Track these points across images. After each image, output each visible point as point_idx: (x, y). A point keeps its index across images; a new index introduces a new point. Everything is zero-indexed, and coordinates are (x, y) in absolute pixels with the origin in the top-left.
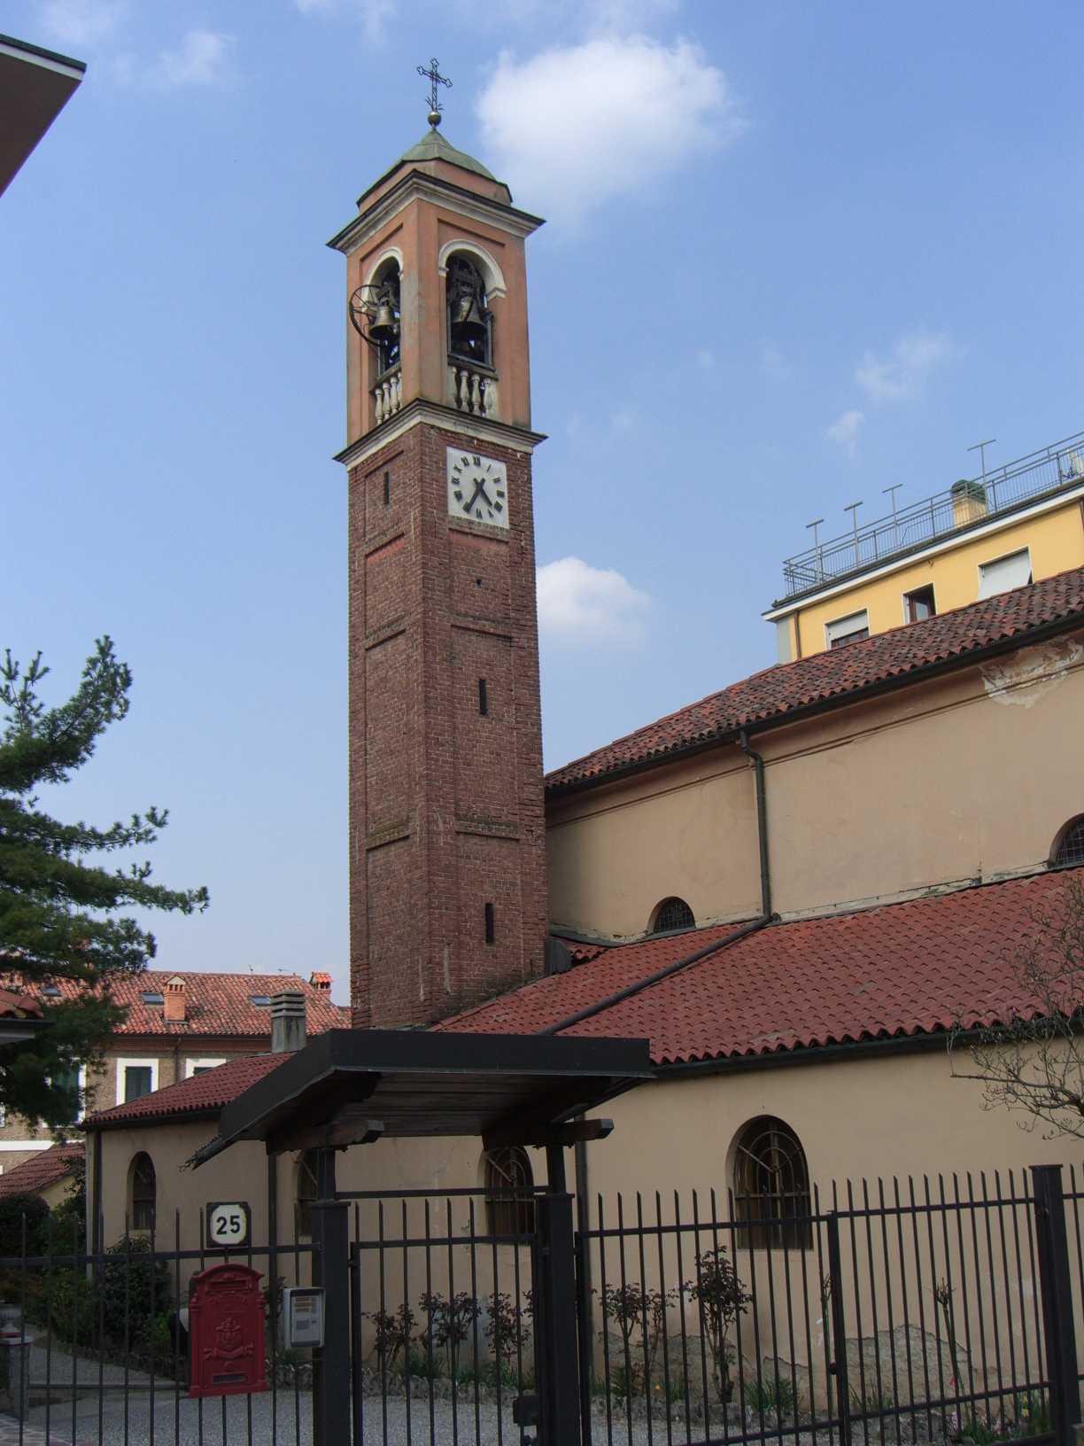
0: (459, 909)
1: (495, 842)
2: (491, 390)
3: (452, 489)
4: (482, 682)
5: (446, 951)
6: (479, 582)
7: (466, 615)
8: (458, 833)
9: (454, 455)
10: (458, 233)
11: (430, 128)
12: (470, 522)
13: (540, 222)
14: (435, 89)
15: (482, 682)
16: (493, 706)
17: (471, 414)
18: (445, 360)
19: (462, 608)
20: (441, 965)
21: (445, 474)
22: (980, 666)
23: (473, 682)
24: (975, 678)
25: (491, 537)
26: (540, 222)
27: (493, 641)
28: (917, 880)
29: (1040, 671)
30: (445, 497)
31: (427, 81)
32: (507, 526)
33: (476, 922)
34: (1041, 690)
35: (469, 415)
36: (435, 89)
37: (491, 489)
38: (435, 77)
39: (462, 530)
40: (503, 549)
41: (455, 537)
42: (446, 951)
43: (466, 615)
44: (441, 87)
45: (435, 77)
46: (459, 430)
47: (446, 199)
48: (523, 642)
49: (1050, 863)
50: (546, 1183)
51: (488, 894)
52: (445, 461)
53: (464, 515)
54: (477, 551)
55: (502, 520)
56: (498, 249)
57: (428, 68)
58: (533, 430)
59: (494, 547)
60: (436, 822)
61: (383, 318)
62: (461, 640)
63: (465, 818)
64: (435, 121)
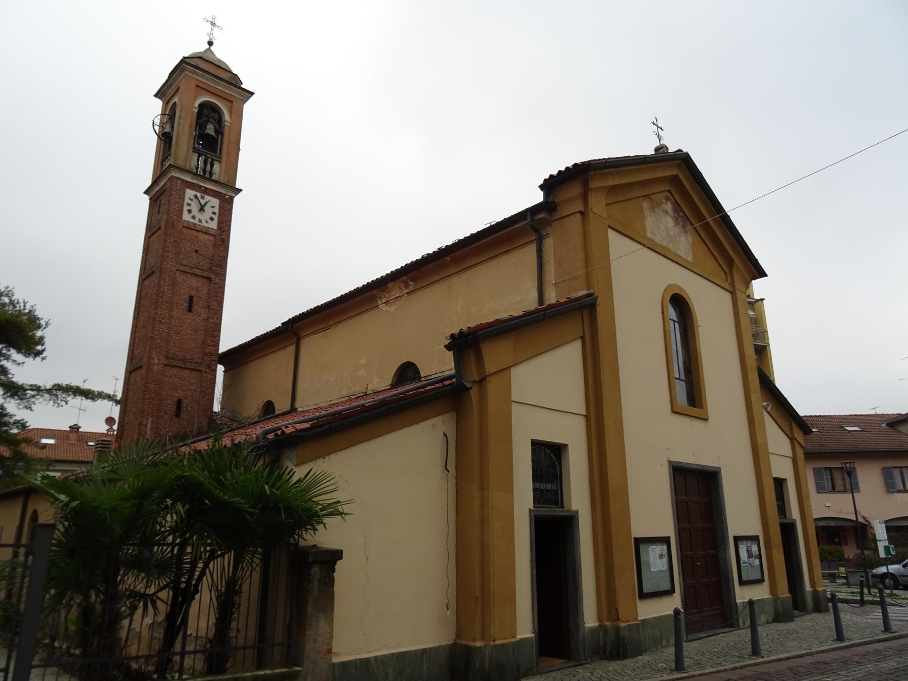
0: (161, 400)
1: (187, 371)
2: (216, 166)
3: (186, 208)
4: (191, 298)
5: (150, 420)
6: (196, 252)
7: (186, 266)
8: (166, 365)
9: (189, 193)
10: (204, 92)
11: (208, 47)
12: (195, 224)
13: (252, 94)
14: (212, 30)
15: (191, 298)
16: (195, 308)
17: (207, 176)
18: (191, 150)
19: (185, 262)
20: (146, 426)
21: (183, 199)
22: (374, 292)
23: (186, 297)
24: (374, 298)
25: (207, 232)
26: (252, 94)
27: (201, 279)
28: (344, 393)
29: (398, 295)
30: (182, 211)
31: (209, 25)
32: (215, 228)
33: (170, 407)
34: (398, 303)
35: (203, 177)
36: (212, 30)
37: (195, 207)
38: (213, 24)
39: (190, 227)
40: (212, 238)
41: (185, 230)
42: (150, 420)
43: (186, 266)
44: (215, 29)
45: (213, 24)
46: (194, 181)
47: (202, 76)
48: (217, 281)
49: (392, 385)
50: (754, 528)
51: (180, 394)
52: (184, 195)
53: (192, 220)
54: (197, 237)
55: (214, 225)
56: (229, 104)
57: (211, 19)
58: (237, 186)
59: (207, 237)
60: (154, 359)
61: (168, 129)
62: (180, 277)
63: (172, 358)
64: (210, 43)
